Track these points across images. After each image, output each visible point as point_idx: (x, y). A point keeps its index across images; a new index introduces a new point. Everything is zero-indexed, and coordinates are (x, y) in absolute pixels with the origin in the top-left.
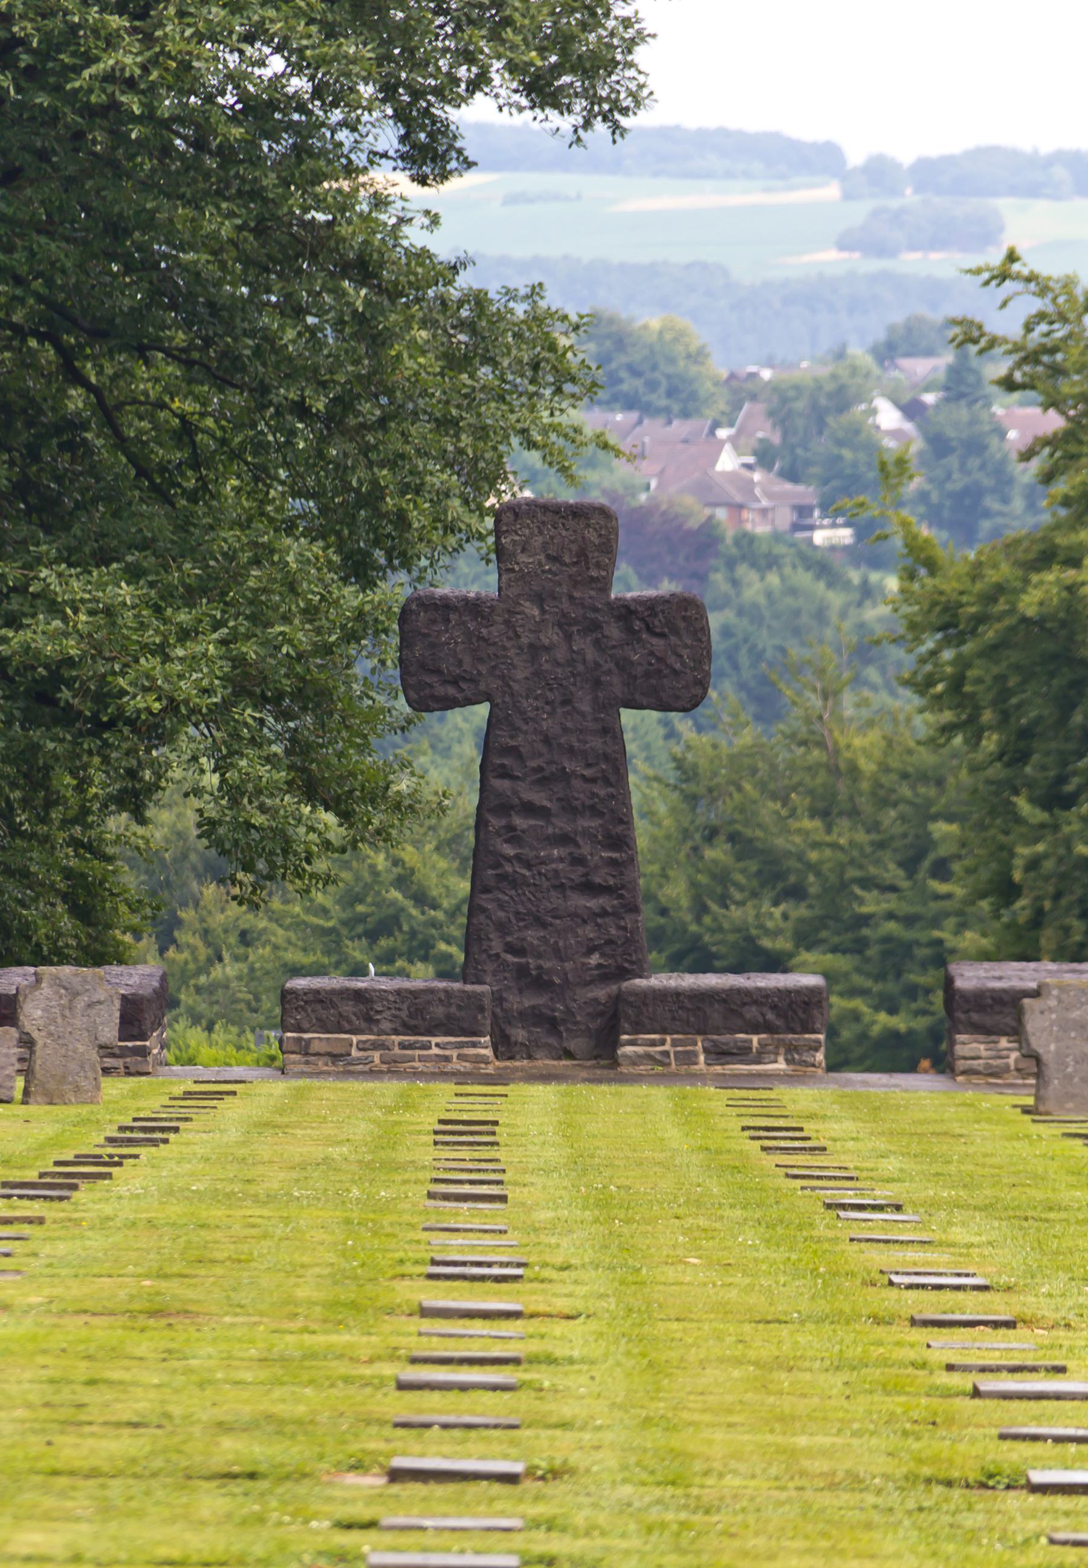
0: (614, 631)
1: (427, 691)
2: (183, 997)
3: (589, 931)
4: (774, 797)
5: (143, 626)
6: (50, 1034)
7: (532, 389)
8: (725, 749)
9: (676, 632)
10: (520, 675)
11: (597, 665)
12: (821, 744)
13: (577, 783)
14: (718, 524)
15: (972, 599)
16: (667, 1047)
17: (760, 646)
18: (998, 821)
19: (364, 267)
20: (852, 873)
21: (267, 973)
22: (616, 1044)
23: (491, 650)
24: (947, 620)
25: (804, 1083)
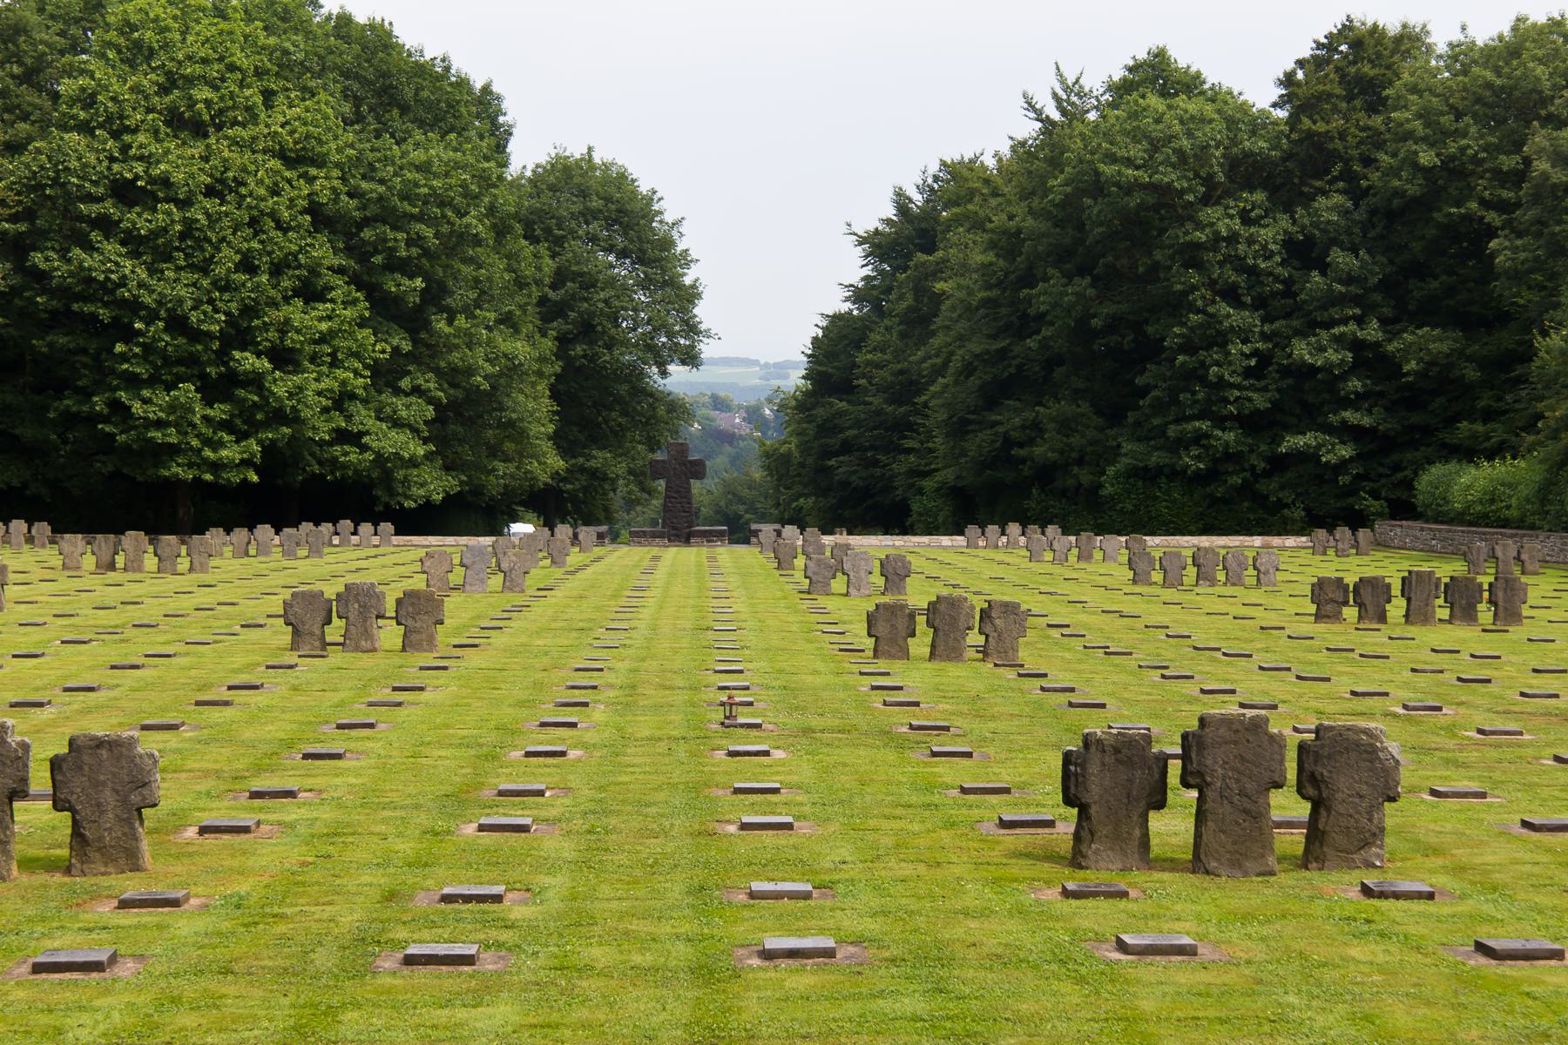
19: (651, 395)
24: (767, 455)
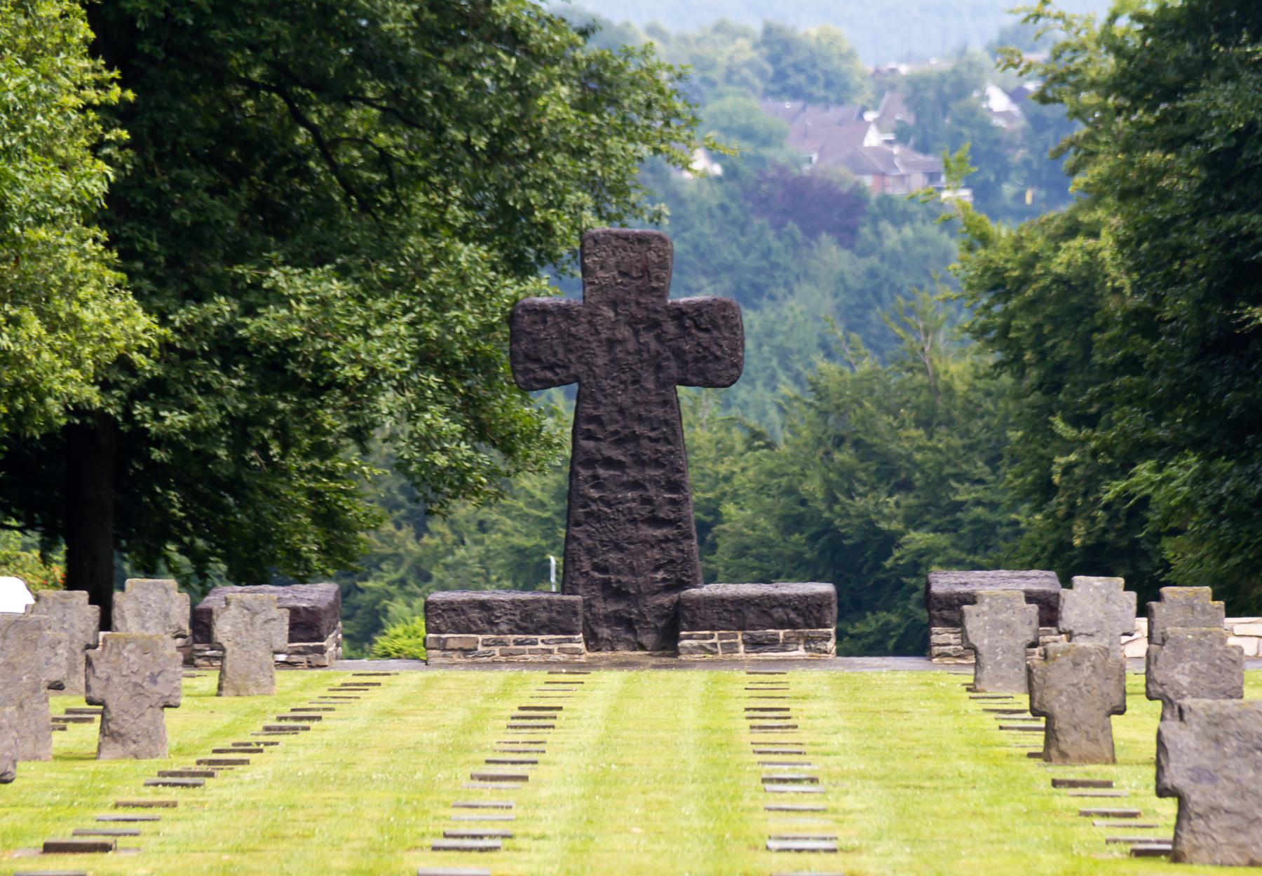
0: (671, 328)
1: (531, 375)
2: (434, 573)
3: (655, 554)
4: (888, 411)
5: (350, 313)
6: (237, 644)
7: (646, 122)
8: (848, 376)
9: (717, 327)
10: (600, 362)
11: (659, 353)
12: (924, 370)
13: (644, 442)
14: (865, 188)
15: (1015, 266)
16: (715, 640)
17: (899, 285)
18: (1039, 437)
20: (948, 470)
21: (499, 554)
22: (677, 638)
23: (578, 344)
25: (815, 665)
